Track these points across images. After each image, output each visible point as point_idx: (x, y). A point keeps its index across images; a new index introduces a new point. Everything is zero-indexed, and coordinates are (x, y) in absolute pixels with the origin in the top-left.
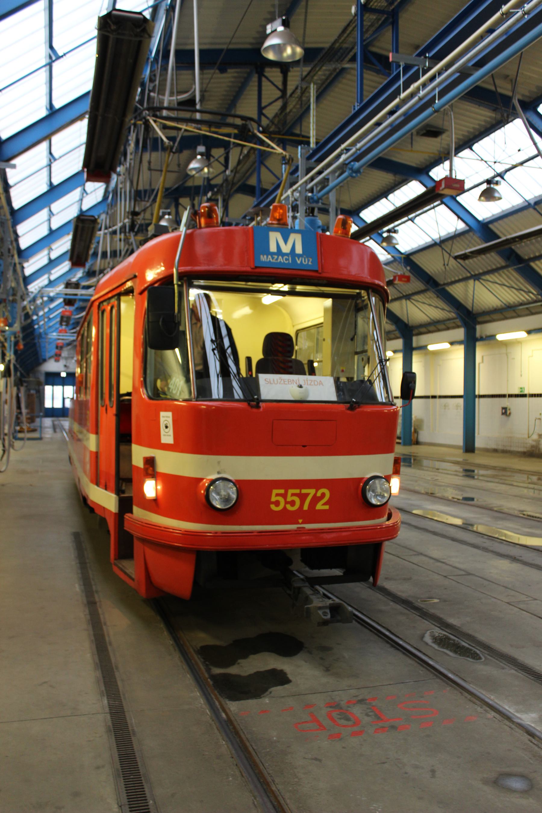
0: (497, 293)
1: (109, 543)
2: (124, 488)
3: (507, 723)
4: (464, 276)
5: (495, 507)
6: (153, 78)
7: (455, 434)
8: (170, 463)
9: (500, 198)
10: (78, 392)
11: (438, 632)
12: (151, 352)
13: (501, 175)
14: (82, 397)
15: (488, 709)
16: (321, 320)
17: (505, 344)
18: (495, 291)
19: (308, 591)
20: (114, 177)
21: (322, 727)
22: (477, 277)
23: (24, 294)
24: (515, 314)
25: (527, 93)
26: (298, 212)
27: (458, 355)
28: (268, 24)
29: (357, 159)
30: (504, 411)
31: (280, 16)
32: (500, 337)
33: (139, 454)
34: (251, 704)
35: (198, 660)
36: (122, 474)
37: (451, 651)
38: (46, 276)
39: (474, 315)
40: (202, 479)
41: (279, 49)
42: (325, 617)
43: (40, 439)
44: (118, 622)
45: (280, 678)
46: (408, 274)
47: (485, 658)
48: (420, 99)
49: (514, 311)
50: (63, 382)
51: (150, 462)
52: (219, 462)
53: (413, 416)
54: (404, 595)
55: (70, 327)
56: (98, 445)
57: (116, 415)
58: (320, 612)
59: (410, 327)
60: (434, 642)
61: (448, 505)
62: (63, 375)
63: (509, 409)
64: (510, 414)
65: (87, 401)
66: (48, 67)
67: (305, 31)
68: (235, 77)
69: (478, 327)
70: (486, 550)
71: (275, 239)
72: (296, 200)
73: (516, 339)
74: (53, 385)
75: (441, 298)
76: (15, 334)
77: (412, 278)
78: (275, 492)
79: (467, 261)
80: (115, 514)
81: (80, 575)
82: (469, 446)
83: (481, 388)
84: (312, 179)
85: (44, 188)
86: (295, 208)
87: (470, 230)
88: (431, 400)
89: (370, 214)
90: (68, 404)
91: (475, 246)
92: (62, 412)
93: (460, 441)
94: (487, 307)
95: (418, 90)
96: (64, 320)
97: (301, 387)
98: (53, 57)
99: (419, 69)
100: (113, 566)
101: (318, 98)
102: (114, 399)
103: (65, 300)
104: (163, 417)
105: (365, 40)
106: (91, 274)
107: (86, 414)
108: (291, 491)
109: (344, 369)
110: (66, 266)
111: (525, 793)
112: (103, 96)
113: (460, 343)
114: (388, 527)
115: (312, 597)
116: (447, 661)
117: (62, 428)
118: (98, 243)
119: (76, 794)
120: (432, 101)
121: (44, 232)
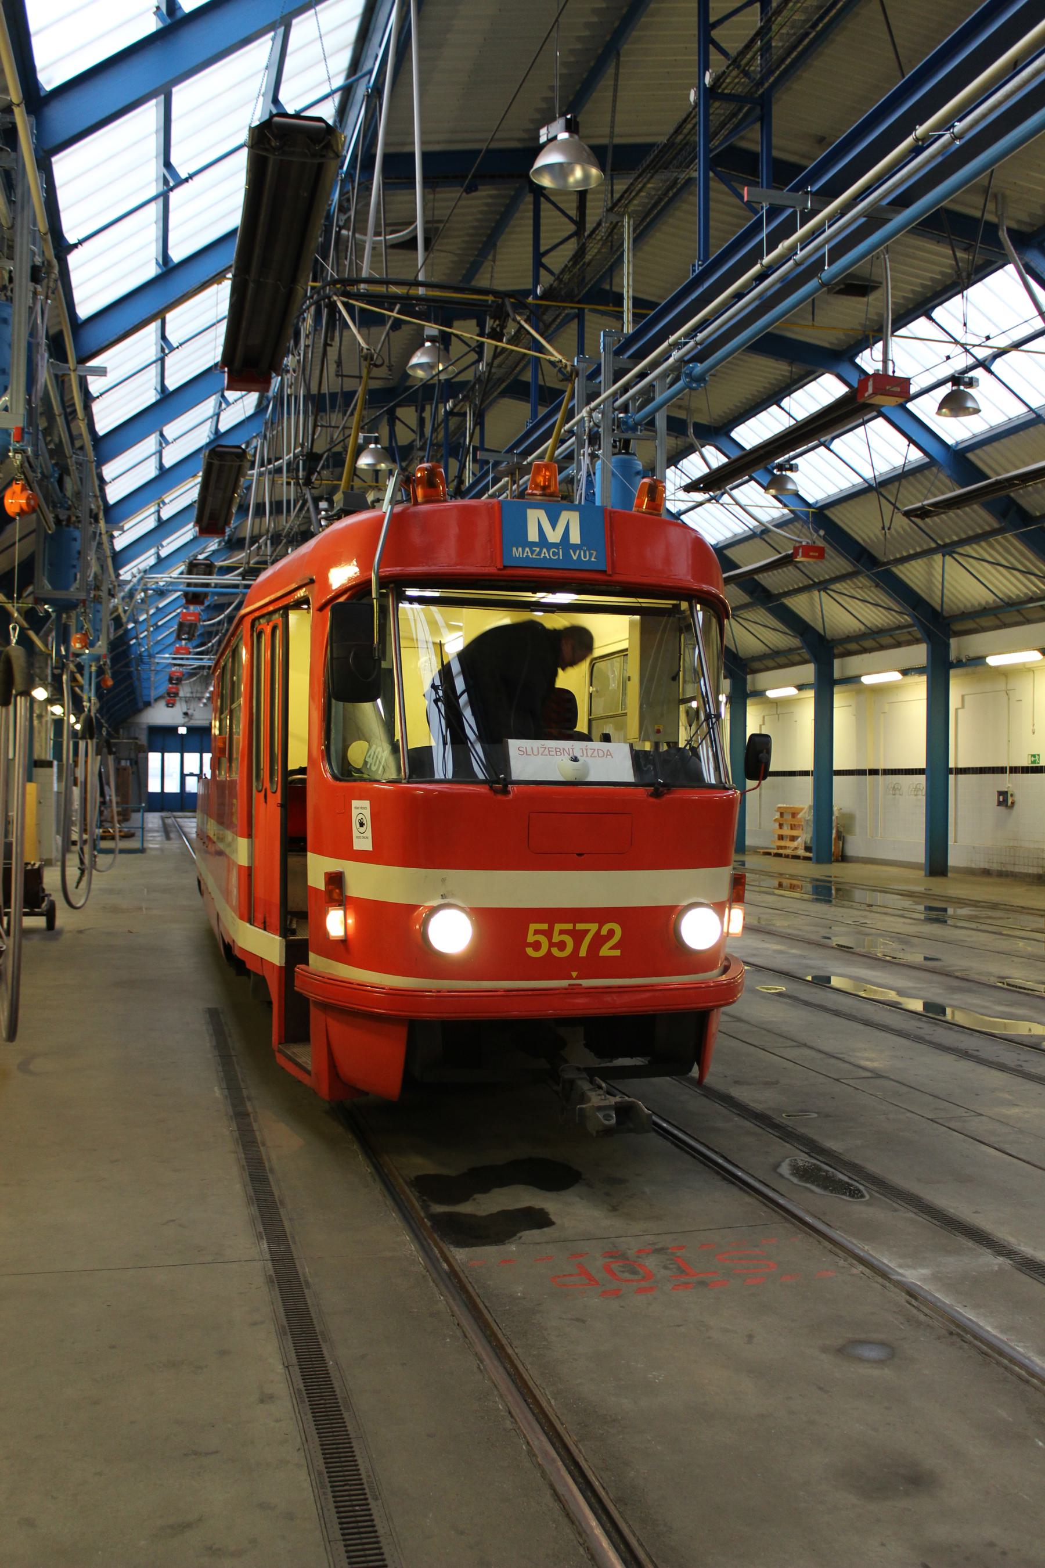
0: (987, 579)
1: (271, 1026)
2: (294, 926)
3: (880, 1280)
4: (925, 547)
5: (957, 971)
6: (345, 204)
7: (909, 841)
8: (368, 881)
9: (977, 411)
10: (215, 765)
11: (803, 1159)
12: (337, 706)
13: (984, 364)
14: (223, 776)
15: (855, 1262)
16: (625, 645)
17: (1004, 673)
18: (984, 577)
19: (585, 1086)
20: (276, 381)
21: (592, 1280)
22: (948, 549)
23: (114, 587)
24: (1020, 618)
25: (1024, 217)
26: (599, 449)
27: (915, 695)
28: (542, 127)
29: (700, 358)
31: (563, 114)
32: (992, 661)
33: (318, 867)
34: (488, 1253)
35: (412, 1196)
36: (292, 905)
37: (818, 1186)
38: (153, 551)
39: (945, 618)
40: (420, 906)
41: (559, 171)
42: (606, 1122)
43: (142, 850)
44: (284, 1141)
45: (539, 1219)
46: (820, 543)
47: (871, 1196)
48: (797, 264)
49: (1018, 611)
50: (182, 746)
51: (336, 880)
52: (444, 880)
53: (835, 809)
54: (759, 1107)
55: (195, 642)
56: (252, 855)
57: (282, 806)
58: (600, 1115)
59: (828, 642)
60: (792, 1174)
61: (872, 968)
62: (182, 731)
64: (1013, 803)
65: (233, 783)
66: (161, 200)
67: (613, 117)
68: (487, 205)
69: (953, 642)
70: (919, 1039)
71: (536, 519)
72: (597, 425)
73: (1024, 664)
74: (163, 751)
75: (881, 588)
76: (97, 659)
77: (829, 551)
78: (533, 927)
79: (928, 520)
80: (280, 967)
81: (221, 1074)
82: (937, 863)
83: (960, 755)
84: (625, 389)
85: (151, 397)
86: (594, 439)
87: (796, 517)
88: (868, 777)
89: (752, 433)
90: (192, 785)
92: (182, 802)
93: (919, 855)
94: (969, 605)
95: (792, 250)
96: (185, 629)
98: (171, 180)
99: (795, 212)
100: (277, 1054)
101: (637, 240)
102: (278, 778)
103: (186, 594)
104: (356, 808)
105: (711, 151)
106: (235, 544)
107: (231, 805)
108: (558, 927)
109: (661, 728)
110: (188, 532)
111: (880, 1363)
112: (257, 251)
113: (919, 671)
114: (719, 986)
115: (590, 1093)
116: (809, 1201)
117: (182, 832)
118: (249, 488)
119: (223, 1353)
120: (815, 268)
121: (150, 471)
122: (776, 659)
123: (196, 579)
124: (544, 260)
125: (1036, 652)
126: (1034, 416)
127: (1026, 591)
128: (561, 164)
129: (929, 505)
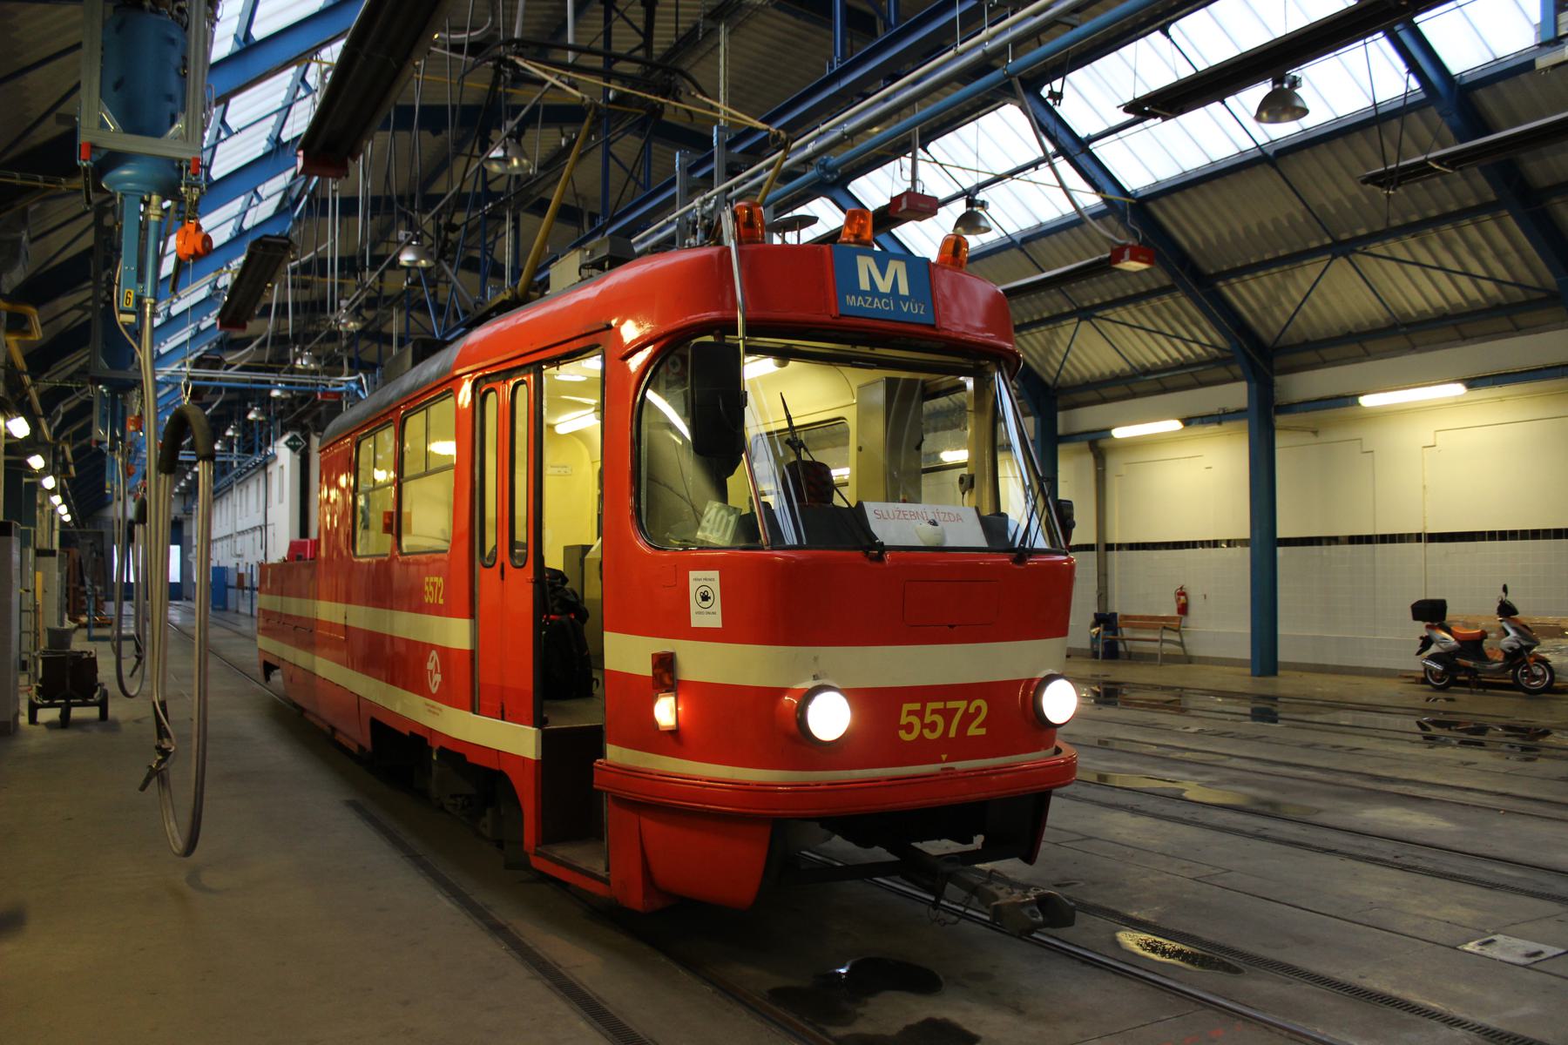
8: (703, 663)
51: (665, 663)
52: (816, 659)
58: (1026, 912)
78: (907, 707)
97: (934, 523)
108: (931, 706)
123: (203, 372)
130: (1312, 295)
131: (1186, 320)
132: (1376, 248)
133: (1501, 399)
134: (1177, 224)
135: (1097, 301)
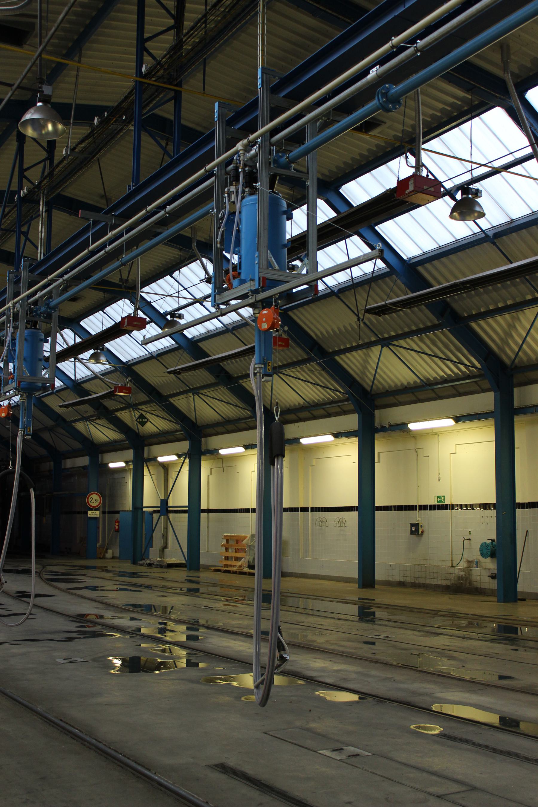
22: (386, 342)
30: (414, 529)
46: (129, 385)
49: (432, 390)
59: (198, 427)
63: (421, 526)
69: (377, 412)
82: (367, 576)
86: (16, 317)
87: (391, 272)
88: (300, 514)
89: (360, 191)
91: (182, 364)
122: (164, 438)
124: (26, 174)
125: (330, 436)
126: (330, 291)
127: (323, 397)
128: (38, 119)
129: (178, 369)
130: (532, 331)
131: (452, 348)
132: (402, 342)
133: (384, 437)
134: (305, 324)
135: (393, 334)
